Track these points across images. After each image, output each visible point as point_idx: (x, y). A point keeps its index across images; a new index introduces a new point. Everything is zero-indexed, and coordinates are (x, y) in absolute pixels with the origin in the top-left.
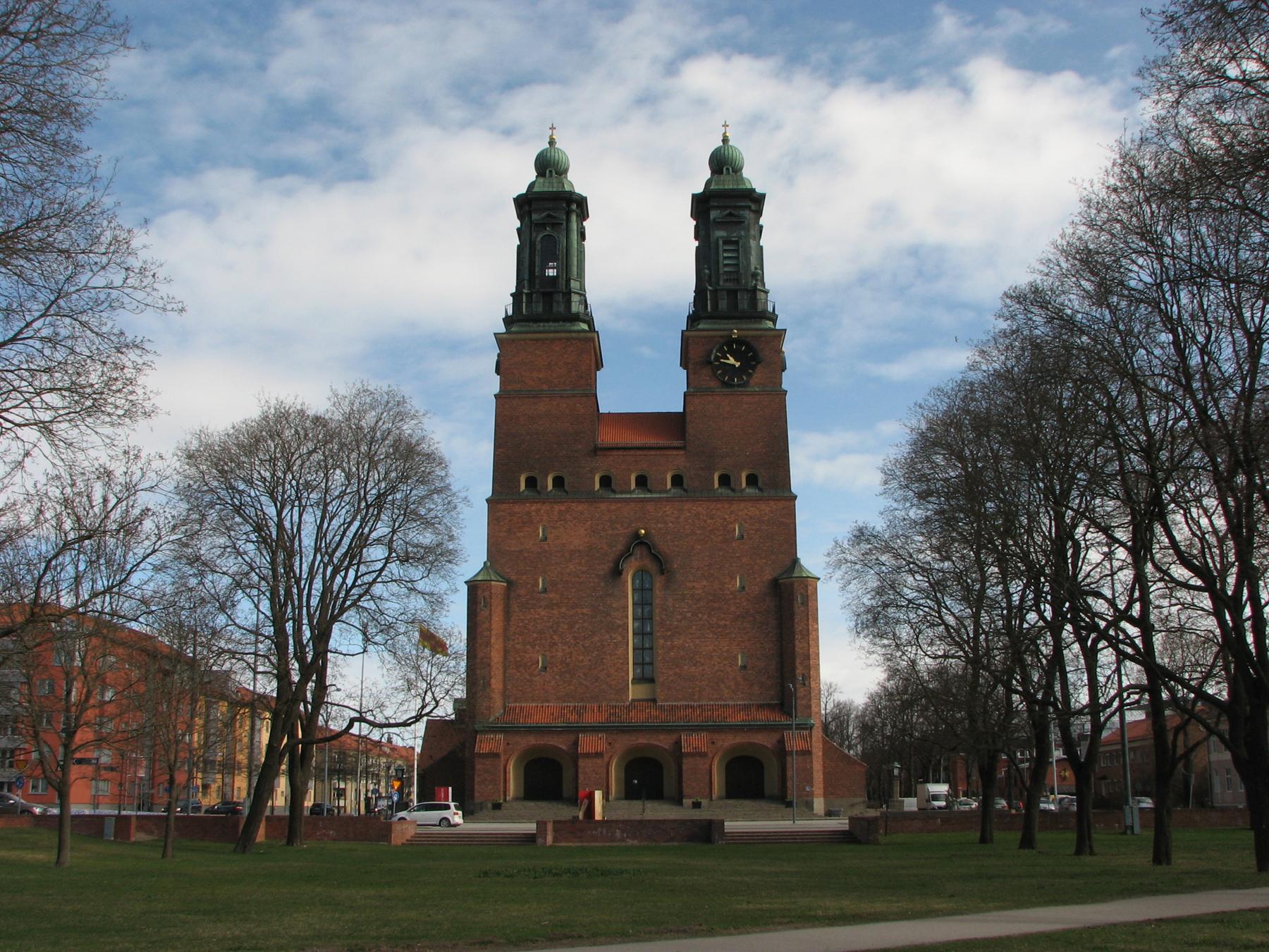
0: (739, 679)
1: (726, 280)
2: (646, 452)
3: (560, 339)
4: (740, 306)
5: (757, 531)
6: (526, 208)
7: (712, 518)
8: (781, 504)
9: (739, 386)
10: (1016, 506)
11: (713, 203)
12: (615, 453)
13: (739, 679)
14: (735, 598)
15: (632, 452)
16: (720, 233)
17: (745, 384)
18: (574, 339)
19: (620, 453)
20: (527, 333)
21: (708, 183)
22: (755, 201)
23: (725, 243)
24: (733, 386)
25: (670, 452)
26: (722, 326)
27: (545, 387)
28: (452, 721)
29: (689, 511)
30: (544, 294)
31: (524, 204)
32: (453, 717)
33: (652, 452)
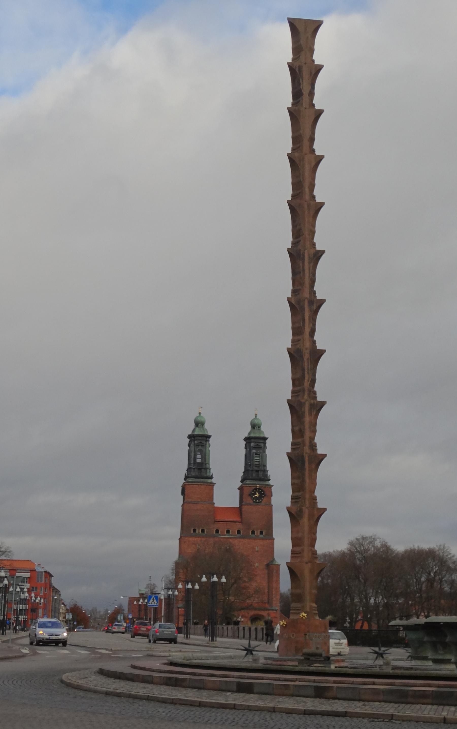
6: (193, 439)
8: (270, 541)
11: (253, 441)
16: (254, 451)
23: (256, 454)
24: (256, 503)
27: (199, 500)
31: (248, 440)
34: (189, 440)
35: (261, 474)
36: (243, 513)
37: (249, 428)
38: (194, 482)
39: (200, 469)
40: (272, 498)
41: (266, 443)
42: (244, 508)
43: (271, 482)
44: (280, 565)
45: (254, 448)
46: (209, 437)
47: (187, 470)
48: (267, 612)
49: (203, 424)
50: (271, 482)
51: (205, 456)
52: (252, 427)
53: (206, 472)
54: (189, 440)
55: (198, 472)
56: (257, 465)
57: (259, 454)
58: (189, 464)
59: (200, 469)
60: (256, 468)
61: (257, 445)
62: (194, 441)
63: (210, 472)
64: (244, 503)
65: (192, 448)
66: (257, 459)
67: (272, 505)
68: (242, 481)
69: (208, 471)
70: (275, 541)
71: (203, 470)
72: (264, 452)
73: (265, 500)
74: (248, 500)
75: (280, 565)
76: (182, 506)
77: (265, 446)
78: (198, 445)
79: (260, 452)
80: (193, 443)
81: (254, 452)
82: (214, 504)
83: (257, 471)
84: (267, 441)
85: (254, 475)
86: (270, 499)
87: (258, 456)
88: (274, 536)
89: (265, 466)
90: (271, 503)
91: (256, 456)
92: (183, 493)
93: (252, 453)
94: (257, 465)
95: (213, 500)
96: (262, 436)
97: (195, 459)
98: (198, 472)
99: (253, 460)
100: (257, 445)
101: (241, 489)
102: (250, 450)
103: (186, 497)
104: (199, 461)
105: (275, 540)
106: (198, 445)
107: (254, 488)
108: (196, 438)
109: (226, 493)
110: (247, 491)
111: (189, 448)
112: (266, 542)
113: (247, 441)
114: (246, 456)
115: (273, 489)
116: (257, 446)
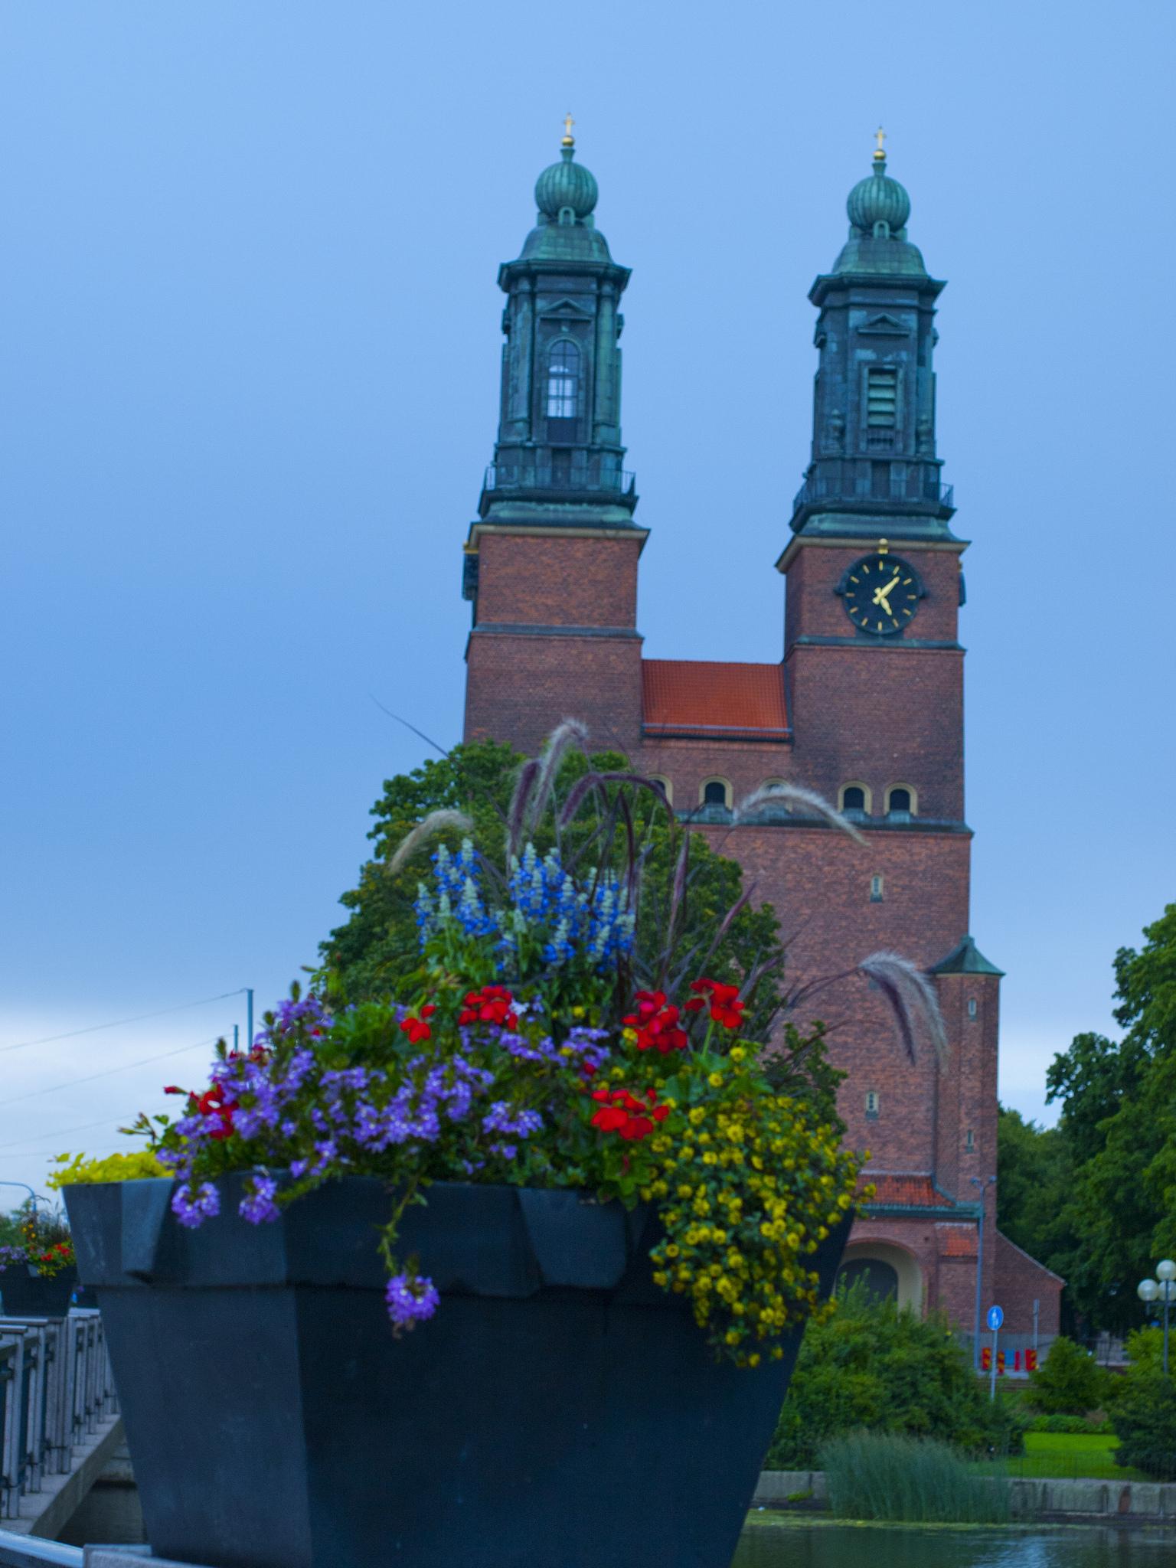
0: (865, 1132)
1: (871, 441)
2: (724, 745)
3: (585, 538)
4: (894, 491)
5: (904, 888)
6: (525, 285)
7: (831, 864)
8: (946, 845)
9: (885, 636)
10: (752, 939)
11: (855, 297)
12: (672, 743)
13: (865, 1132)
14: (864, 1000)
15: (703, 745)
16: (866, 354)
17: (897, 634)
18: (608, 539)
19: (682, 744)
20: (525, 523)
21: (531, 242)
22: (615, 279)
23: (874, 372)
24: (875, 635)
25: (765, 747)
26: (868, 528)
27: (557, 623)
28: (215, 1217)
29: (794, 849)
30: (557, 451)
31: (828, 293)
32: (217, 1212)
33: (736, 746)
34: (816, 312)
35: (899, 478)
36: (799, 689)
37: (839, 233)
38: (525, 523)
39: (560, 453)
40: (962, 611)
41: (933, 313)
42: (808, 665)
43: (956, 527)
44: (1002, 975)
45: (867, 337)
46: (619, 278)
47: (496, 463)
48: (925, 1230)
49: (584, 208)
50: (956, 527)
51: (599, 387)
52: (855, 224)
53: (597, 468)
54: (816, 312)
55: (559, 474)
56: (883, 434)
57: (893, 373)
58: (506, 424)
59: (560, 453)
60: (878, 451)
61: (566, 305)
62: (532, 296)
63: (619, 468)
64: (804, 639)
65: (522, 338)
66: (883, 401)
67: (963, 651)
68: (799, 522)
69: (609, 461)
70: (978, 849)
71: (580, 458)
72: (922, 360)
73: (921, 621)
74: (839, 623)
75: (1002, 975)
76: (466, 658)
77: (925, 335)
78: (557, 322)
79: (898, 363)
80: (526, 307)
81: (861, 363)
82: (640, 640)
83: (881, 465)
84: (939, 304)
85: (864, 486)
86: (954, 616)
87: (888, 380)
88: (971, 820)
89: (925, 435)
90: (954, 635)
91: (878, 380)
92: (472, 588)
93: (852, 366)
94: (883, 434)
95: (632, 622)
96: (909, 270)
97: (537, 398)
98: (559, 474)
99: (858, 407)
100: (884, 320)
101: (790, 563)
102: (844, 353)
103: (483, 602)
104: (560, 405)
105: (974, 843)
106: (552, 322)
107: (861, 555)
108: (542, 283)
109: (712, 585)
110: (824, 576)
111: (504, 339)
112: (923, 850)
113: (833, 299)
114: (819, 383)
115: (968, 561)
116: (880, 329)
